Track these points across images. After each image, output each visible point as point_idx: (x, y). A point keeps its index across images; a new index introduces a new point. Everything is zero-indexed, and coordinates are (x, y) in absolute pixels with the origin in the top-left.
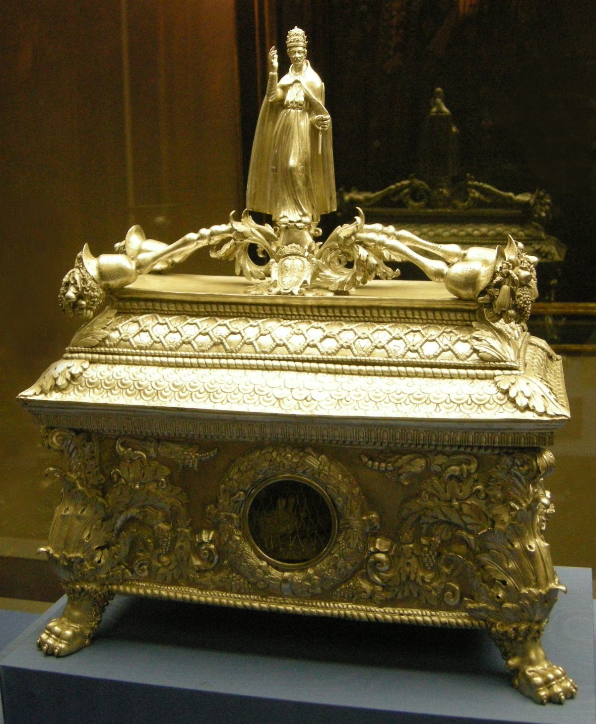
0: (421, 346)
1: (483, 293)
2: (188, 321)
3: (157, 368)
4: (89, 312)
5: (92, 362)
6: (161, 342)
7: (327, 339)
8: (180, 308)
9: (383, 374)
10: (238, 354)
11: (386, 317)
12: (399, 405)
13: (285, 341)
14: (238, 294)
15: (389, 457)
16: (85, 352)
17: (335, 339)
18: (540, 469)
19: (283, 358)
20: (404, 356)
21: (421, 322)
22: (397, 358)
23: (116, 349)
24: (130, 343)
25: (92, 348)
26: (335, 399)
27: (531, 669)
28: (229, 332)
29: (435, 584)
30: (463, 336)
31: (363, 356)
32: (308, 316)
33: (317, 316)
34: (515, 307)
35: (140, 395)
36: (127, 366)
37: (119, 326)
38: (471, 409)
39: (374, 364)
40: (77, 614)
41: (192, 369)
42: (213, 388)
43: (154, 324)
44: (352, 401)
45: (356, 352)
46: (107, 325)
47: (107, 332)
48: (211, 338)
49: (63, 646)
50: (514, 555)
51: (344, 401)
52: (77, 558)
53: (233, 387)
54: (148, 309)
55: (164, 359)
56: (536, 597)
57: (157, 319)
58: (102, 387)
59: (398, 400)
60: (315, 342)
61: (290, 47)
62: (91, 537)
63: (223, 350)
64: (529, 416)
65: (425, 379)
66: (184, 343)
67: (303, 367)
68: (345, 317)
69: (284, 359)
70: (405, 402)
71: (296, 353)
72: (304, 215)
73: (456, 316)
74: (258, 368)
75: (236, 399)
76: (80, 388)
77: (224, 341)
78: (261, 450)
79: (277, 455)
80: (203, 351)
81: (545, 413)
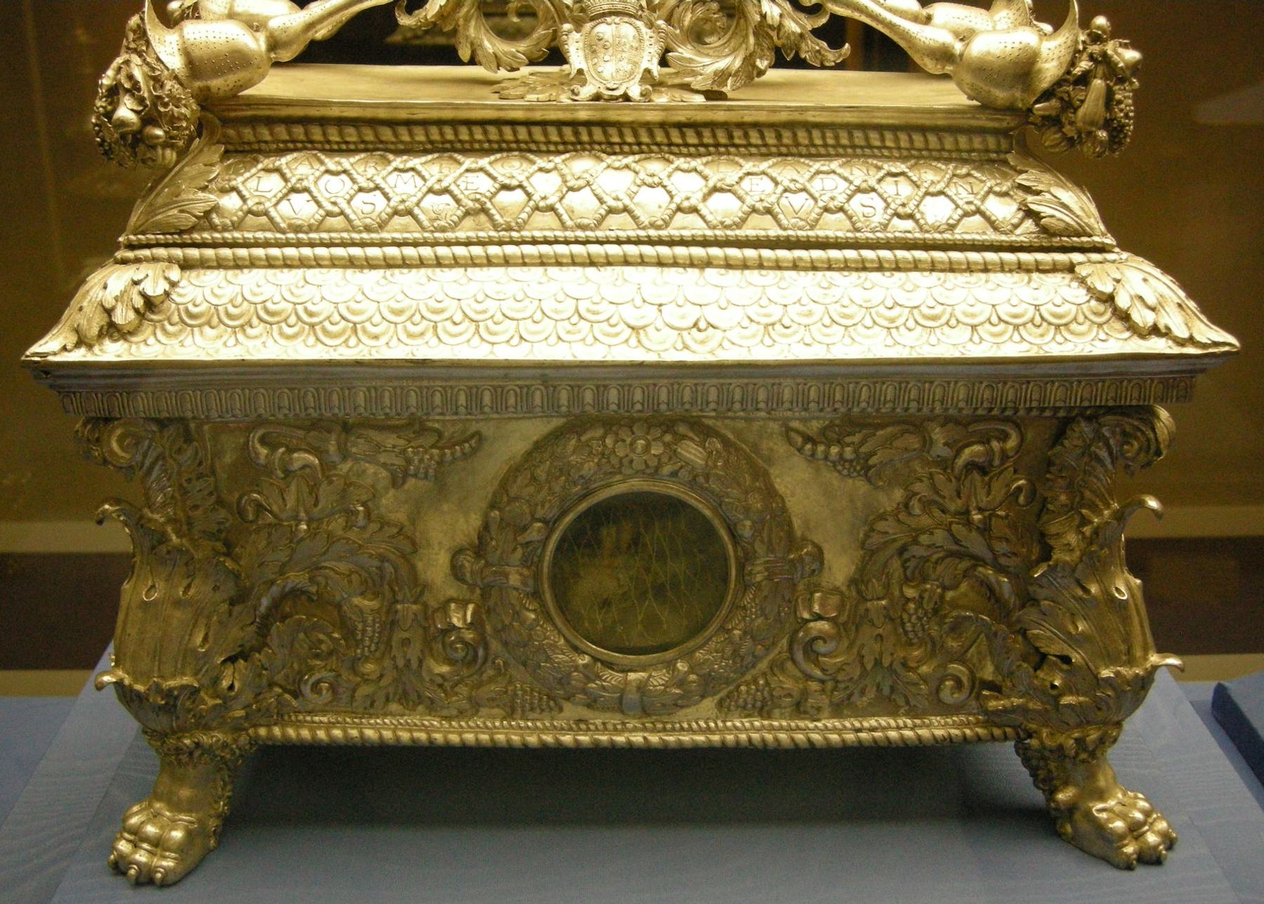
0: (917, 206)
1: (1047, 95)
2: (394, 165)
3: (340, 271)
4: (168, 152)
5: (186, 265)
6: (342, 213)
7: (717, 195)
8: (369, 135)
9: (846, 267)
10: (524, 233)
11: (825, 145)
12: (893, 331)
13: (627, 201)
14: (485, 103)
16: (166, 245)
17: (735, 193)
18: (1162, 446)
20: (885, 227)
22: (873, 231)
23: (237, 235)
24: (271, 219)
25: (180, 236)
26: (758, 323)
27: (1100, 806)
28: (497, 186)
29: (924, 669)
30: (997, 184)
31: (801, 229)
33: (678, 145)
34: (1107, 124)
35: (315, 334)
36: (270, 272)
37: (238, 182)
38: (1042, 336)
39: (824, 244)
40: (185, 793)
41: (423, 271)
42: (484, 312)
43: (317, 174)
44: (795, 326)
45: (784, 222)
46: (210, 181)
47: (212, 197)
48: (458, 201)
49: (169, 863)
50: (1088, 606)
51: (778, 327)
52: (183, 687)
53: (531, 308)
54: (293, 141)
56: (1128, 683)
57: (322, 163)
58: (221, 321)
59: (892, 320)
60: (693, 202)
62: (211, 640)
63: (488, 225)
65: (935, 274)
66: (396, 212)
68: (737, 146)
69: (629, 241)
70: (905, 324)
71: (653, 225)
73: (971, 140)
74: (574, 262)
75: (503, 332)
77: (489, 205)
78: (579, 435)
79: (616, 442)
80: (443, 230)
81: (1191, 340)
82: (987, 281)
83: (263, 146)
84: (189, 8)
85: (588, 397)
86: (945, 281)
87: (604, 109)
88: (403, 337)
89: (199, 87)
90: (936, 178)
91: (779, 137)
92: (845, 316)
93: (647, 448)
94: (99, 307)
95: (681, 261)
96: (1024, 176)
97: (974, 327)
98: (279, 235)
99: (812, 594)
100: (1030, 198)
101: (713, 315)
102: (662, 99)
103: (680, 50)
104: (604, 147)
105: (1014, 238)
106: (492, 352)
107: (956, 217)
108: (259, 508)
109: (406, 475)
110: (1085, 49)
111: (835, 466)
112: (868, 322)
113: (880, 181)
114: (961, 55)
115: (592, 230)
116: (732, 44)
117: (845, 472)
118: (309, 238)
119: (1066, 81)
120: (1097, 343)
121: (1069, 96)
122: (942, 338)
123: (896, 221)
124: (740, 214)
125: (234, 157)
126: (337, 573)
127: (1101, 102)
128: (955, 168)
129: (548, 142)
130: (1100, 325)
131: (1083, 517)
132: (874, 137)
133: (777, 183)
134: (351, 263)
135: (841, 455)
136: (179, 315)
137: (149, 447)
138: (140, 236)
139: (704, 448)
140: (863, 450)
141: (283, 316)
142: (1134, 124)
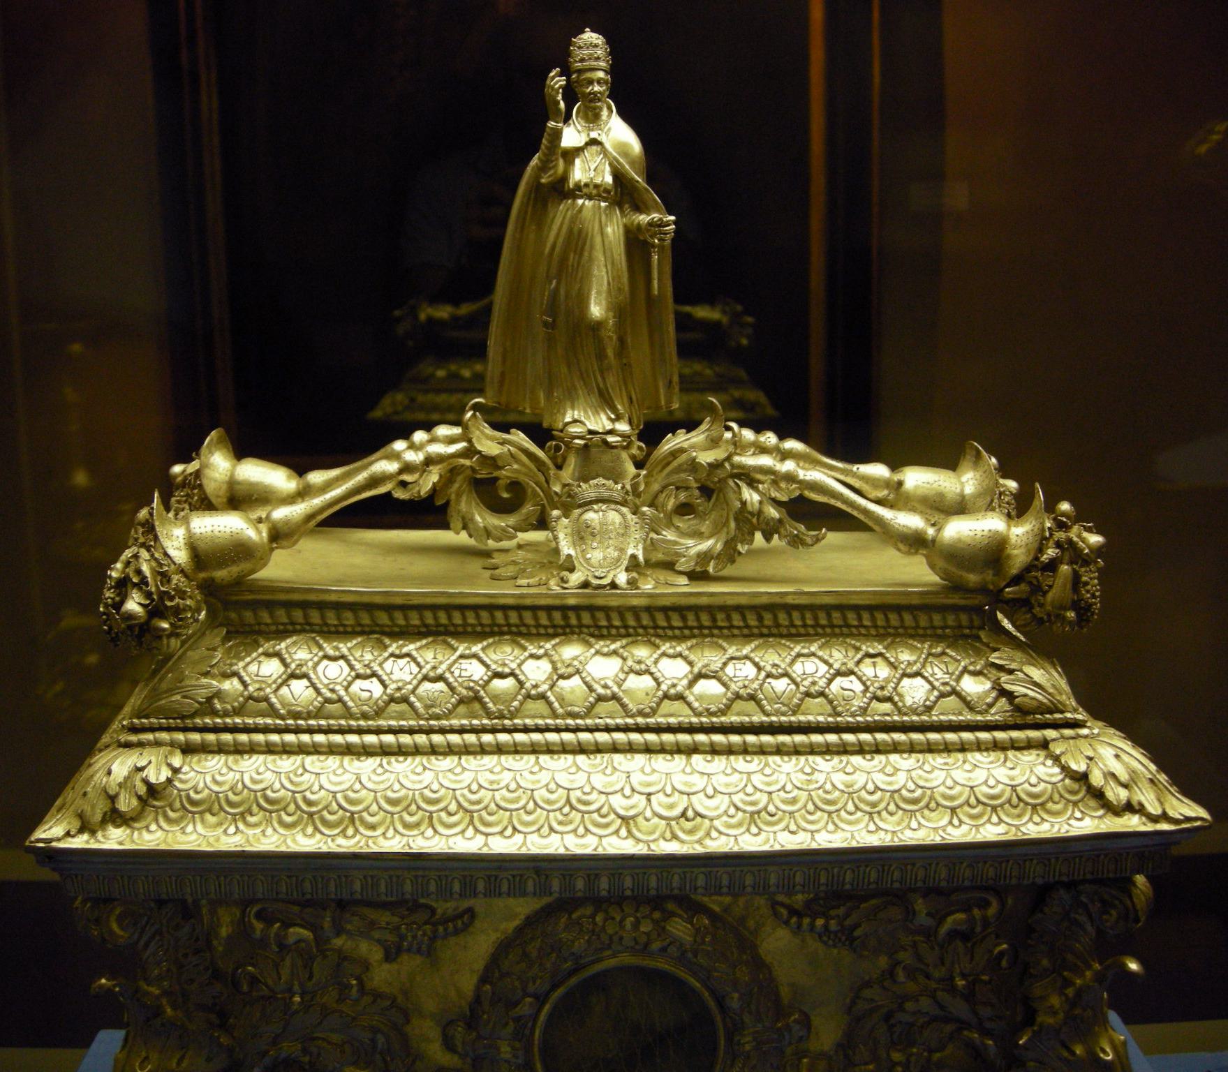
0: (895, 689)
1: (1017, 580)
2: (390, 650)
3: (338, 758)
5: (188, 750)
6: (340, 700)
9: (827, 750)
10: (517, 721)
11: (805, 626)
13: (615, 689)
15: (833, 908)
16: (169, 729)
19: (617, 725)
20: (864, 710)
21: (873, 632)
22: (853, 715)
24: (271, 705)
26: (744, 811)
30: (971, 663)
31: (784, 714)
32: (645, 628)
34: (1075, 606)
36: (270, 758)
41: (418, 759)
42: (479, 802)
43: (316, 659)
46: (212, 667)
48: (452, 688)
55: (353, 739)
57: (321, 648)
58: (221, 808)
59: (874, 805)
61: (580, 71)
64: (1133, 823)
67: (662, 744)
68: (720, 628)
70: (886, 809)
71: (641, 713)
72: (618, 418)
74: (564, 749)
76: (171, 814)
77: (482, 693)
79: (606, 920)
80: (438, 717)
81: (1165, 817)
82: (964, 762)
83: (263, 628)
84: (191, 474)
85: (580, 884)
86: (924, 763)
87: (593, 596)
88: (400, 828)
89: (203, 579)
90: (913, 658)
91: (760, 619)
92: (829, 802)
93: (636, 925)
94: (103, 796)
95: (668, 748)
96: (996, 654)
97: (953, 810)
98: (278, 722)
99: (800, 1059)
100: (1004, 678)
101: (700, 803)
102: (648, 586)
103: (664, 533)
104: (592, 630)
105: (989, 718)
106: (486, 844)
107: (932, 698)
108: (254, 980)
109: (399, 950)
110: (1051, 535)
111: (820, 936)
112: (850, 807)
113: (858, 663)
114: (934, 541)
115: (582, 718)
116: (713, 516)
117: (831, 942)
118: (308, 725)
119: (1035, 566)
120: (1072, 822)
121: (1038, 581)
122: (923, 821)
123: (875, 704)
124: (724, 701)
125: (236, 638)
126: (329, 1043)
127: (1069, 586)
128: (930, 647)
129: (538, 626)
130: (1075, 804)
131: (1065, 979)
132: (852, 618)
133: (759, 668)
134: (348, 750)
135: (826, 926)
136: (181, 802)
137: (147, 923)
138: (143, 720)
139: (692, 924)
140: (848, 922)
141: (283, 805)
142: (1100, 602)
